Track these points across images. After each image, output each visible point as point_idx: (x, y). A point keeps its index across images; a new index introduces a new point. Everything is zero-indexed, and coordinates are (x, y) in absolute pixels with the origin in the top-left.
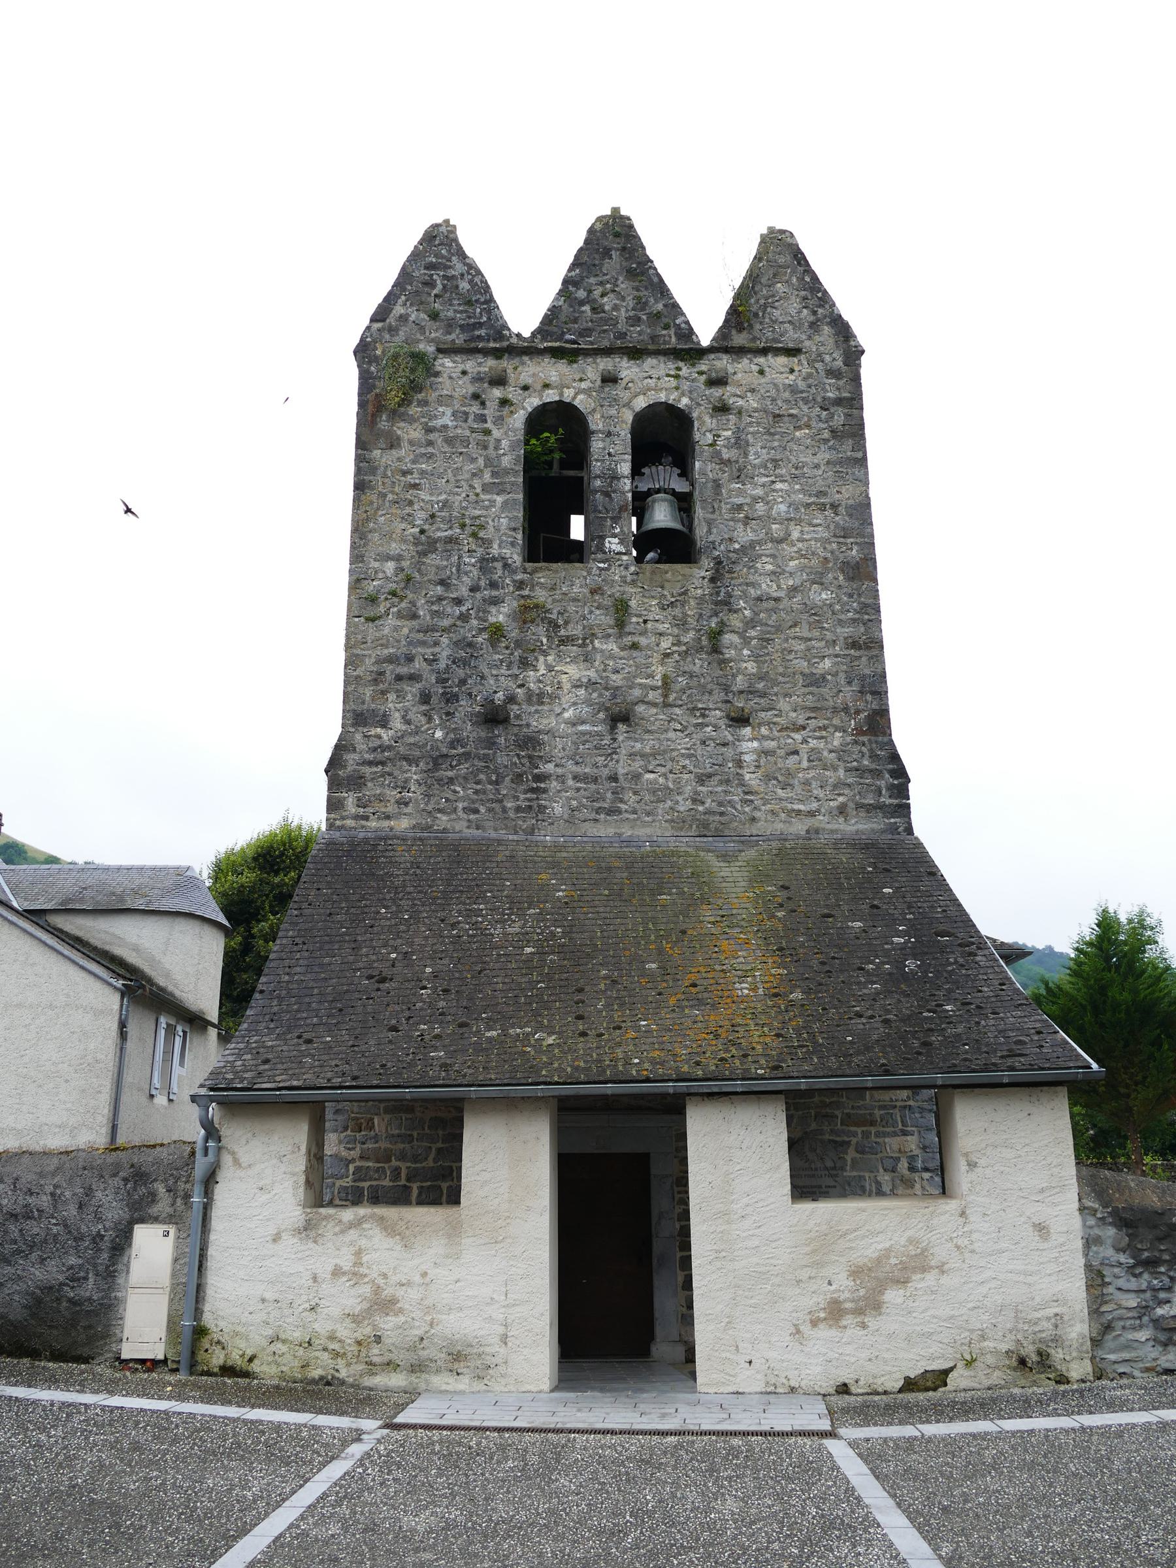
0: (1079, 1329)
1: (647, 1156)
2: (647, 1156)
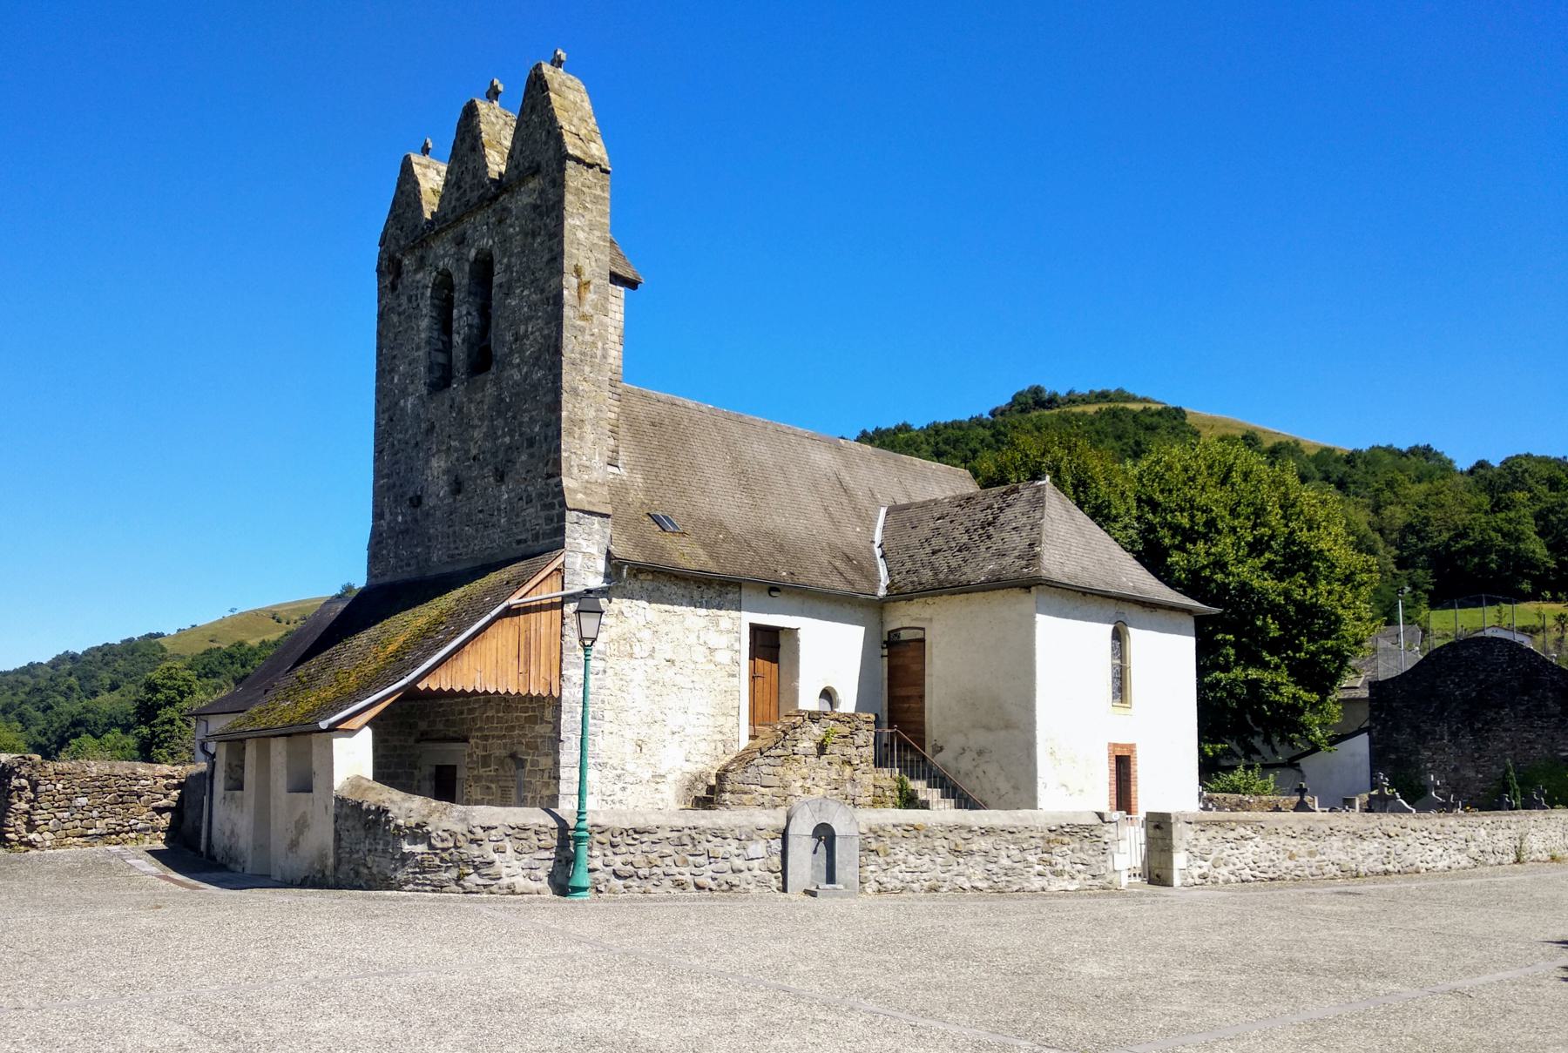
0: (331, 861)
1: (455, 767)
2: (455, 767)
